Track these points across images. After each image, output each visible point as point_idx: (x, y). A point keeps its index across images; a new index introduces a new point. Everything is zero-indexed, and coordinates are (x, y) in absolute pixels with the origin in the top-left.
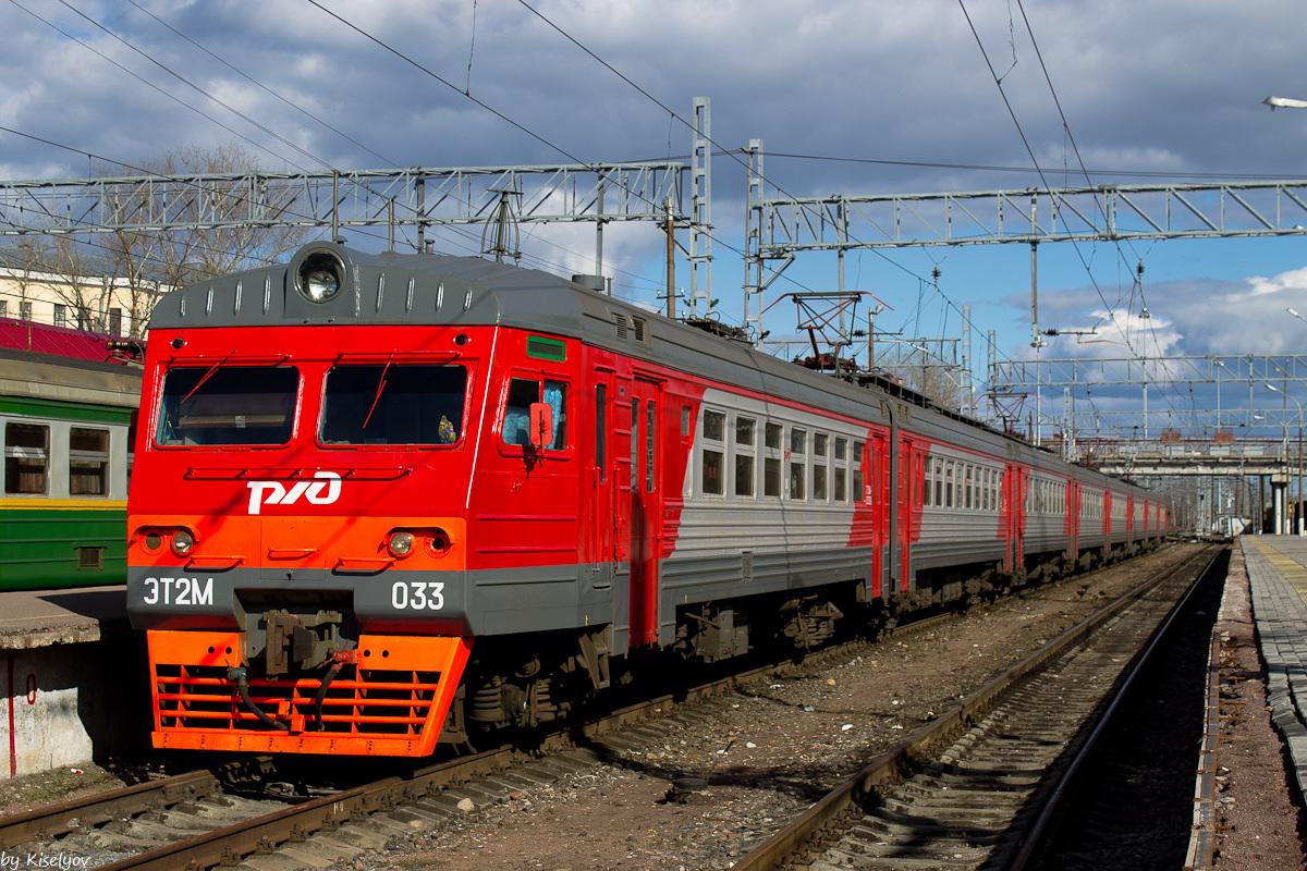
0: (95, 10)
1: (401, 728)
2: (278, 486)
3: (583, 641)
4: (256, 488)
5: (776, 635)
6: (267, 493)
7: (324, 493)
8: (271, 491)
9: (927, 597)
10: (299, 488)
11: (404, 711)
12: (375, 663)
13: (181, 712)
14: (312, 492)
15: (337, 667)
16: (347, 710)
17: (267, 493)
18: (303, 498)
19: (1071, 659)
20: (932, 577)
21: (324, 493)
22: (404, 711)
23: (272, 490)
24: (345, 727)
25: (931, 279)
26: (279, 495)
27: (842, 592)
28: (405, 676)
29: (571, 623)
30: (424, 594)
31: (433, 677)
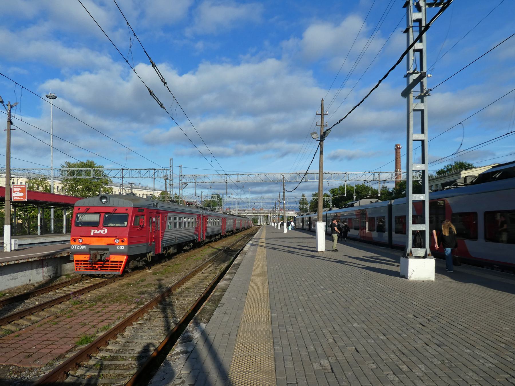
0: (472, 385)
1: (117, 270)
2: (96, 231)
3: (147, 255)
4: (92, 231)
5: (474, 222)
6: (94, 231)
7: (104, 232)
8: (103, 232)
9: (207, 240)
10: (100, 231)
11: (117, 267)
12: (112, 260)
13: (119, 263)
14: (102, 232)
15: (106, 260)
16: (108, 267)
17: (94, 231)
18: (100, 233)
19: (58, 359)
20: (210, 237)
21: (104, 232)
22: (117, 267)
23: (103, 232)
24: (107, 270)
25: (242, 188)
26: (96, 232)
27: (193, 241)
28: (117, 262)
29: (145, 252)
30: (121, 247)
31: (122, 262)
